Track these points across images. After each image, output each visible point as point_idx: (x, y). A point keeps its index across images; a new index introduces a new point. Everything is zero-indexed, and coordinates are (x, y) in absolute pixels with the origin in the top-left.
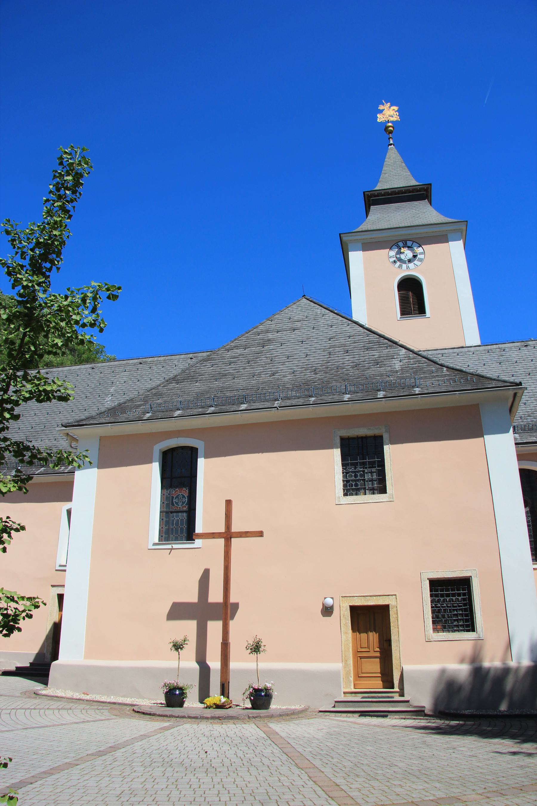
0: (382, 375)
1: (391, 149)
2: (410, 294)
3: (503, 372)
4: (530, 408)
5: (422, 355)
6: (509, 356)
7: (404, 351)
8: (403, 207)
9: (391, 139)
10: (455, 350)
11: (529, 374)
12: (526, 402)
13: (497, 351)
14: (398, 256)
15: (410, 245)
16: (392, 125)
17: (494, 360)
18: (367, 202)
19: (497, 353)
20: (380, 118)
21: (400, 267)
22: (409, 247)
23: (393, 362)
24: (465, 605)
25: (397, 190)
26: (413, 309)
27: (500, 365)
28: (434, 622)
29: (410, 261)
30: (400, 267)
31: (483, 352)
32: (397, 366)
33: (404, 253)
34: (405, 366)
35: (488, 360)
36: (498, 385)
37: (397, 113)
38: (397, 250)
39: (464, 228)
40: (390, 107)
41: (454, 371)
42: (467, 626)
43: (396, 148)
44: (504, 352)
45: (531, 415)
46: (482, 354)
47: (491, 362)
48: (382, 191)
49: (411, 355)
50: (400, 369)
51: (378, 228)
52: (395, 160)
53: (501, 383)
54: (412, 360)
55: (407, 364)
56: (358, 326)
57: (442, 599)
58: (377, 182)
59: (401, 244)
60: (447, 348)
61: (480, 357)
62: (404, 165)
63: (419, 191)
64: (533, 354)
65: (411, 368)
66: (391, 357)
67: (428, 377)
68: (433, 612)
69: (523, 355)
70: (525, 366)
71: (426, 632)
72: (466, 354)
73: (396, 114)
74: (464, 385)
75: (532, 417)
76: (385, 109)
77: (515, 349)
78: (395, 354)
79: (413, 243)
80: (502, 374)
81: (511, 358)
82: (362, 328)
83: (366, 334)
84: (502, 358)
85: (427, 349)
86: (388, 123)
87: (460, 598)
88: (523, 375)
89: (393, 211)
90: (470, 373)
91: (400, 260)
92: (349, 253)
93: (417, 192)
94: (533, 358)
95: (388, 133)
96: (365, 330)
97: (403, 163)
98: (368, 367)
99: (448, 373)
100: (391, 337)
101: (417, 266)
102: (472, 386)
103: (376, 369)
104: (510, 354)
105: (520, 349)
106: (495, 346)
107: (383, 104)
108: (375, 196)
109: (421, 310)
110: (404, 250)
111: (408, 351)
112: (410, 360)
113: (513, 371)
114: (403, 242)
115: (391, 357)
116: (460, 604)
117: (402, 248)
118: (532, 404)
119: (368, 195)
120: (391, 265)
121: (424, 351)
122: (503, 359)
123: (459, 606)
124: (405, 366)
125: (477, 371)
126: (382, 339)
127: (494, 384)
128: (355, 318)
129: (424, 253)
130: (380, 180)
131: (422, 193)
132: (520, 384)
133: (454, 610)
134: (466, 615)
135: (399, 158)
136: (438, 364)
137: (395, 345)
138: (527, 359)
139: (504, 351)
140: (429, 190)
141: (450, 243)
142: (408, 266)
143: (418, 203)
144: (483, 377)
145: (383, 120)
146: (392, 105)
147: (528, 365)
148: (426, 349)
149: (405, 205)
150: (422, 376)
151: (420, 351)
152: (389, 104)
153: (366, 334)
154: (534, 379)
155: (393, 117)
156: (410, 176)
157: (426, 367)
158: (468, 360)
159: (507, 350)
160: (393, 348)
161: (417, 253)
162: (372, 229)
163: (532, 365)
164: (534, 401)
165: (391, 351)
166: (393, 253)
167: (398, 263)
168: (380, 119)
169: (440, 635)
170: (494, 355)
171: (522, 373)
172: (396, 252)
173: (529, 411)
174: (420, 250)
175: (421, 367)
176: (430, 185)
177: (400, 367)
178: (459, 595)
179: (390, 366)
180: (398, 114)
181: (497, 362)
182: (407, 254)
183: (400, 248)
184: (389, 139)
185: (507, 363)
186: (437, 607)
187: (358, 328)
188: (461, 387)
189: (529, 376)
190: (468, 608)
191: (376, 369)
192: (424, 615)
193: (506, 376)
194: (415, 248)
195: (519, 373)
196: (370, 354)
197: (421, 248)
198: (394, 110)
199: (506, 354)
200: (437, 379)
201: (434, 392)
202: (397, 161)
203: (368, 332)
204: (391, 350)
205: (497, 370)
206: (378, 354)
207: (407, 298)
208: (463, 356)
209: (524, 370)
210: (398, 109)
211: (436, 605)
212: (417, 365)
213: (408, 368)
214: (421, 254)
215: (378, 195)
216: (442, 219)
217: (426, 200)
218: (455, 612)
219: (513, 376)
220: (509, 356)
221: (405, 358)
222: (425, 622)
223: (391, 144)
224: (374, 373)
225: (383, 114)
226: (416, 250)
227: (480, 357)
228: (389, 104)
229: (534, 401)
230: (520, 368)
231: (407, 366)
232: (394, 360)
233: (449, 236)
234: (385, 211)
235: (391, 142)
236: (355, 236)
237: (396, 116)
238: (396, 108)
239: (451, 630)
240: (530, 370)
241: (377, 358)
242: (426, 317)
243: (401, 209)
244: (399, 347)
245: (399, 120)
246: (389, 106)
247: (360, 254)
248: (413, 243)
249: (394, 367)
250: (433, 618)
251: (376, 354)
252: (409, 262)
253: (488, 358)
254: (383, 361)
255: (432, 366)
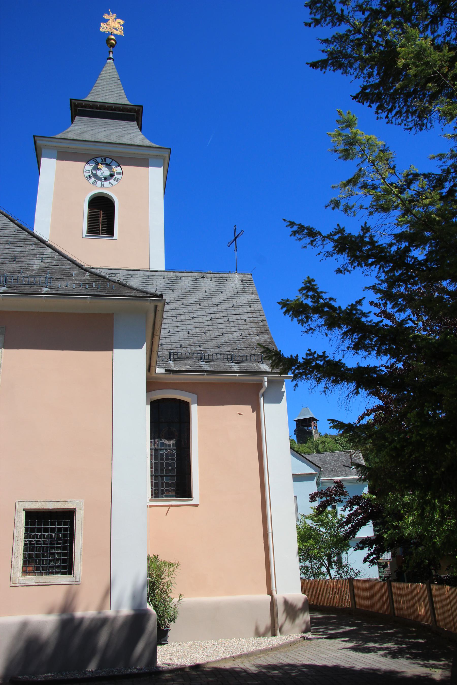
0: (14, 271)
1: (110, 63)
2: (101, 213)
3: (173, 299)
4: (192, 337)
5: (68, 258)
6: (184, 285)
7: (50, 251)
8: (110, 124)
9: (111, 53)
10: (130, 272)
11: (200, 305)
12: (190, 331)
13: (173, 278)
14: (94, 172)
15: (109, 163)
16: (115, 39)
17: (167, 286)
18: (73, 110)
19: (173, 280)
20: (104, 28)
21: (94, 183)
22: (107, 165)
23: (33, 261)
24: (65, 542)
25: (106, 105)
26: (102, 229)
27: (173, 293)
28: (25, 563)
29: (106, 179)
30: (94, 183)
31: (158, 278)
32: (36, 264)
33: (101, 169)
34: (45, 266)
35: (161, 286)
36: (136, 295)
37: (122, 27)
38: (94, 165)
39: (167, 155)
40: (115, 19)
41: (97, 276)
42: (64, 567)
43: (115, 64)
44: (180, 281)
45: (192, 344)
46: (157, 280)
47: (164, 288)
48: (90, 102)
49: (56, 257)
50: (38, 268)
51: (78, 139)
52: (111, 75)
53: (141, 293)
54: (55, 262)
55: (48, 264)
56: (9, 220)
57: (39, 534)
58: (88, 92)
59: (99, 160)
60: (122, 268)
61: (154, 282)
62: (119, 82)
63: (130, 111)
64: (208, 286)
65: (51, 269)
66: (33, 256)
67: (64, 280)
68: (26, 550)
69: (198, 286)
70: (198, 296)
71: (12, 574)
72: (141, 277)
73: (121, 28)
74: (100, 291)
75: (192, 347)
76: (111, 20)
77: (192, 279)
78: (38, 253)
79: (112, 161)
80: (173, 301)
81: (185, 287)
82: (12, 223)
83: (14, 229)
84: (176, 286)
85: (101, 267)
86: (112, 35)
87: (60, 534)
88: (193, 305)
89: (99, 126)
90: (113, 280)
91: (95, 176)
92: (42, 159)
93: (127, 112)
94: (218, 303)
95: (109, 46)
96: (15, 225)
97: (120, 80)
98: (2, 262)
99: (89, 278)
100: (40, 235)
101: (112, 185)
102: (108, 293)
103: (10, 265)
104: (186, 283)
105: (196, 280)
106: (172, 274)
107: (109, 14)
108: (82, 107)
109: (110, 231)
110: (101, 167)
111: (55, 252)
112: (52, 261)
113: (184, 300)
114: (101, 158)
115: (33, 256)
116: (60, 540)
117: (100, 164)
118: (195, 333)
119: (74, 103)
120: (85, 180)
121: (96, 269)
122: (177, 287)
123: (58, 544)
124: (45, 266)
125: (120, 279)
126: (31, 236)
127: (133, 293)
128: (37, 230)
129: (121, 173)
130: (91, 91)
131: (132, 114)
132: (161, 296)
133: (51, 548)
134: (65, 555)
135: (116, 74)
136: (82, 269)
137: (42, 244)
138: (201, 290)
139: (180, 279)
140: (140, 113)
141: (150, 168)
142: (103, 184)
143: (127, 123)
144: (124, 285)
145: (107, 30)
146: (118, 17)
147: (201, 296)
148: (99, 267)
149: (113, 122)
150: (59, 277)
151: (93, 268)
152: (115, 15)
153: (14, 229)
154: (203, 310)
155: (117, 30)
156: (124, 95)
157: (68, 269)
158: (140, 283)
159: (184, 279)
160: (39, 246)
161: (115, 173)
162: (72, 138)
163: (205, 296)
164: (198, 331)
165: (35, 249)
166: (89, 167)
167: (93, 179)
168: (103, 28)
169: (29, 579)
170: (169, 282)
171: (192, 302)
172: (92, 167)
173: (191, 340)
174: (118, 169)
175: (62, 269)
176: (141, 107)
177: (38, 266)
178: (59, 530)
179: (28, 264)
180: (123, 29)
181: (170, 289)
182: (105, 171)
183: (98, 164)
184: (110, 52)
185: (180, 291)
186: (31, 544)
187: (8, 222)
188: (96, 292)
189: (200, 307)
190: (68, 545)
191: (10, 265)
192: (13, 554)
193: (176, 304)
194: (113, 167)
195: (190, 302)
196: (10, 250)
197: (120, 167)
198: (119, 23)
199: (182, 283)
200: (74, 282)
201: (63, 293)
202: (113, 77)
203: (18, 227)
204: (36, 248)
205: (168, 297)
206: (20, 250)
207: (97, 217)
208: (137, 279)
209: (195, 300)
210: (124, 24)
211: (30, 541)
212: (58, 267)
213: (48, 268)
214: (118, 173)
215: (85, 106)
216: (146, 142)
217: (136, 122)
218: (53, 551)
219: (183, 305)
220: (184, 285)
221: (48, 259)
222: (13, 562)
223: (110, 59)
224: (6, 269)
225: (107, 25)
226: (114, 169)
227: (154, 282)
228: (115, 15)
229: (198, 331)
230: (192, 298)
231: (47, 266)
232: (35, 258)
233: (151, 161)
234: (90, 124)
235: (111, 56)
236: (51, 141)
237: (121, 31)
238: (122, 22)
239: (44, 572)
240: (202, 300)
241: (16, 255)
242: (113, 239)
243: (107, 125)
244: (46, 246)
245: (123, 35)
246: (115, 17)
247: (54, 162)
248: (112, 161)
249: (32, 265)
250: (24, 557)
251: (17, 250)
252: (104, 180)
253: (162, 284)
254: (22, 258)
255: (75, 270)
